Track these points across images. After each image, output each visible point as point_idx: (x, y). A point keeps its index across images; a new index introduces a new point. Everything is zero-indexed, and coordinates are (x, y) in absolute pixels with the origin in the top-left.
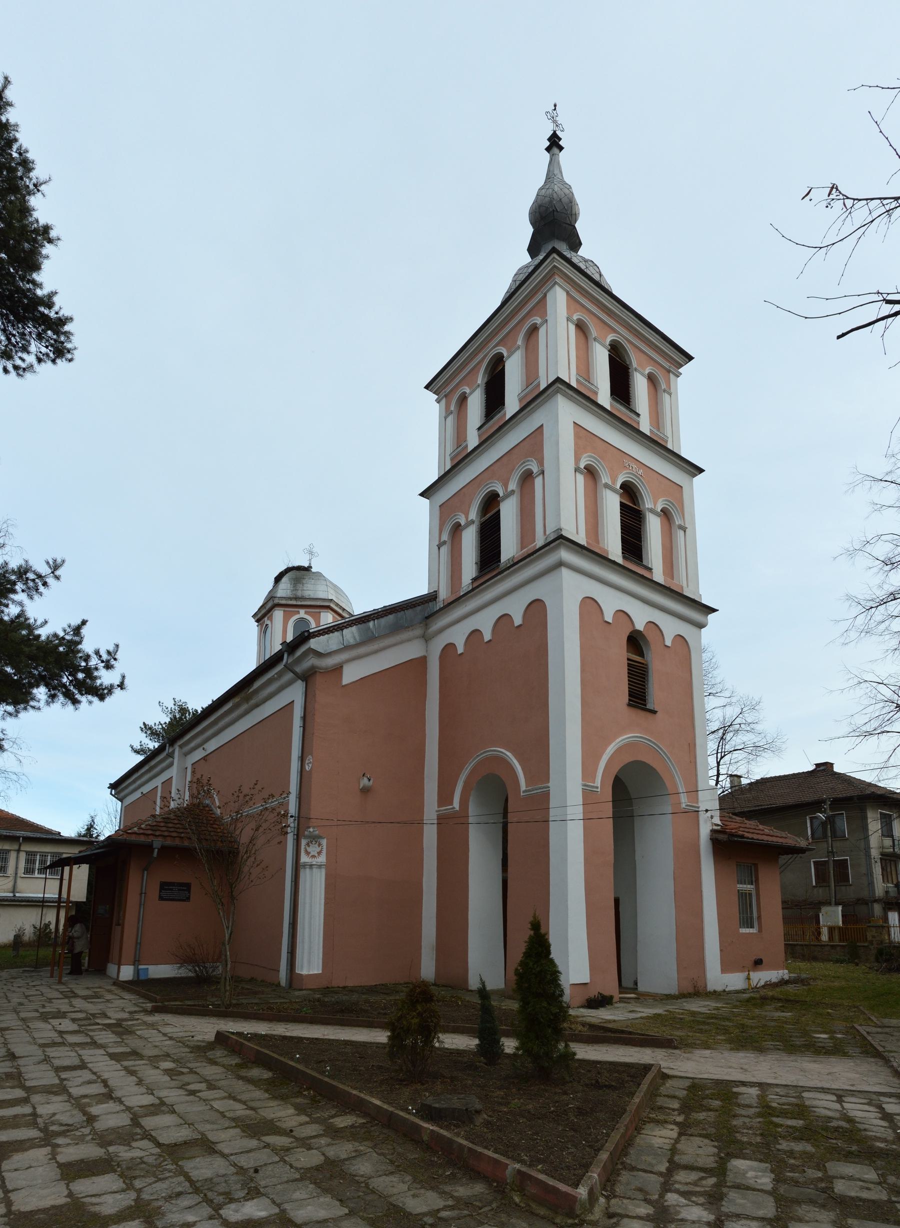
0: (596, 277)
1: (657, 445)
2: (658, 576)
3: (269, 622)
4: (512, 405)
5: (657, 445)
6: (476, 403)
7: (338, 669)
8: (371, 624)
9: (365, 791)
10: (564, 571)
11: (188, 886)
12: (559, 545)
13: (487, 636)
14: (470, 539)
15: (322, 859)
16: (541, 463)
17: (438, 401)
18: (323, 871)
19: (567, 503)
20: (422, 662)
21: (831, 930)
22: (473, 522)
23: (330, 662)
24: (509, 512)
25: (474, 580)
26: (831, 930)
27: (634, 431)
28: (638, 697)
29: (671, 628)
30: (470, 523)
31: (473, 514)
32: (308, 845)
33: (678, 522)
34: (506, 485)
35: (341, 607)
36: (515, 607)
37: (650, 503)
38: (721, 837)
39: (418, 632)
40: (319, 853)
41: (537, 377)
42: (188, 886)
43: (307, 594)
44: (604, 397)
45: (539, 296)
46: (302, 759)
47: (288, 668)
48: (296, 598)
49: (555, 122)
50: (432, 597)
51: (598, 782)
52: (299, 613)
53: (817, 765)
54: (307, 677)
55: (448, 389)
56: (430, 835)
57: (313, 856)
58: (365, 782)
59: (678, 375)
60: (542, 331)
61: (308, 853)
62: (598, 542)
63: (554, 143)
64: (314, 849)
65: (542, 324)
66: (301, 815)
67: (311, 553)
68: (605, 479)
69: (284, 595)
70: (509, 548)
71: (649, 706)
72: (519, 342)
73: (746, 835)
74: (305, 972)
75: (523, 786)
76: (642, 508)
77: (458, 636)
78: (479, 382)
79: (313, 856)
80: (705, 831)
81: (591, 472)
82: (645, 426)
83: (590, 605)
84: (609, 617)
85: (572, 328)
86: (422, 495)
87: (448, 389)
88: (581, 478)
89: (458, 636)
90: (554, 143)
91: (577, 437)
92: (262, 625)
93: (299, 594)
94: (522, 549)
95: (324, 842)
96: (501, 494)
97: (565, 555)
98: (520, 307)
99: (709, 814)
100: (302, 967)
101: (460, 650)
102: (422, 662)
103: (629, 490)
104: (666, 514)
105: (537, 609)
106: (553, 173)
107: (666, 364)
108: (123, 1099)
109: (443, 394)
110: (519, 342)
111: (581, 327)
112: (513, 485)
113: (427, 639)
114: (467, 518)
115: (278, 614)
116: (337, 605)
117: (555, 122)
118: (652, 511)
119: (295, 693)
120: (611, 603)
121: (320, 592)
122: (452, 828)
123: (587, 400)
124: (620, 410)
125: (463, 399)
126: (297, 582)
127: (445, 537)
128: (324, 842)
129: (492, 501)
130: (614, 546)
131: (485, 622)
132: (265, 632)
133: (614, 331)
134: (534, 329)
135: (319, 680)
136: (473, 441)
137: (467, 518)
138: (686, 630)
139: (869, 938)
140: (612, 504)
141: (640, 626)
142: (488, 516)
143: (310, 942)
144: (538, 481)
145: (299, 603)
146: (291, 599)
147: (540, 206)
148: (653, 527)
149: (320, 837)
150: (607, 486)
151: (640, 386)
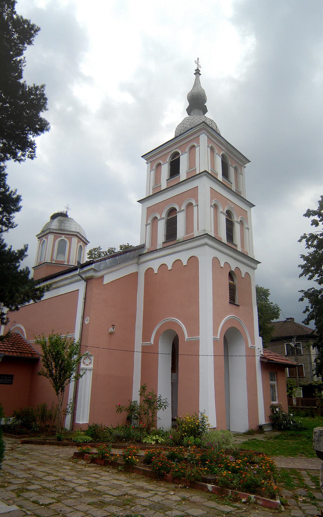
0: (214, 128)
1: (238, 195)
2: (239, 249)
3: (45, 240)
4: (183, 175)
5: (238, 195)
6: (165, 169)
7: (102, 277)
8: (117, 257)
9: (111, 334)
10: (206, 246)
11: (12, 376)
12: (205, 237)
13: (170, 268)
14: (162, 226)
15: (91, 366)
16: (197, 201)
17: (147, 163)
18: (92, 372)
19: (205, 219)
20: (136, 274)
21: (298, 399)
22: (163, 218)
23: (99, 274)
24: (181, 219)
25: (164, 243)
26: (298, 399)
27: (229, 190)
28: (232, 300)
29: (244, 270)
30: (161, 219)
31: (164, 215)
32: (85, 359)
33: (246, 226)
34: (180, 208)
35: (82, 236)
36: (184, 258)
37: (236, 219)
38: (264, 360)
39: (135, 261)
40: (90, 363)
41: (195, 166)
42: (12, 376)
43: (66, 228)
44: (220, 177)
45: (196, 135)
46: (83, 318)
47: (79, 275)
48: (61, 230)
49: (198, 64)
50: (142, 247)
51: (218, 337)
52: (61, 237)
53: (287, 319)
54: (87, 280)
55: (152, 160)
56: (138, 357)
57: (87, 365)
58: (111, 330)
59: (245, 167)
60: (197, 149)
61: (84, 363)
62: (217, 234)
63: (197, 72)
64: (87, 361)
65: (197, 147)
66: (82, 344)
67: (68, 208)
68: (221, 209)
69: (55, 228)
70: (181, 233)
71: (237, 303)
72: (187, 150)
73: (274, 359)
74: (81, 423)
75: (186, 337)
76: (233, 220)
77: (155, 265)
78: (168, 161)
79: (87, 365)
80: (258, 359)
81: (215, 206)
82: (234, 189)
83: (215, 261)
84: (222, 265)
85: (209, 149)
86: (142, 157)
87: (152, 160)
88: (212, 209)
89: (155, 265)
90: (197, 72)
91: (211, 193)
92: (41, 241)
93: (62, 228)
94: (187, 234)
95: (92, 358)
96: (178, 210)
97: (206, 240)
98: (186, 135)
99: (259, 350)
100: (79, 420)
101: (156, 272)
102: (136, 274)
103: (229, 213)
104: (241, 223)
105: (193, 260)
106: (197, 83)
107: (241, 163)
108: (76, 488)
109: (149, 161)
110: (187, 150)
111: (212, 149)
112: (183, 207)
113: (138, 264)
114: (161, 216)
115: (51, 237)
116: (80, 234)
117: (198, 64)
118: (237, 222)
119: (81, 286)
120: (223, 260)
121: (73, 228)
122: (149, 354)
123: (212, 177)
124: (226, 182)
125: (159, 165)
126: (61, 222)
127: (149, 222)
128: (92, 358)
129: (173, 211)
130: (223, 237)
131: (169, 262)
132: (42, 244)
133: (223, 150)
134: (194, 146)
135: (93, 283)
136: (164, 186)
137: (161, 216)
138: (249, 270)
139: (317, 405)
140: (223, 219)
141: (233, 269)
142: (171, 217)
143: (84, 407)
144: (195, 209)
145: (62, 232)
146: (58, 230)
147: (192, 96)
148: (237, 228)
149: (91, 356)
150: (221, 212)
151: (232, 171)
